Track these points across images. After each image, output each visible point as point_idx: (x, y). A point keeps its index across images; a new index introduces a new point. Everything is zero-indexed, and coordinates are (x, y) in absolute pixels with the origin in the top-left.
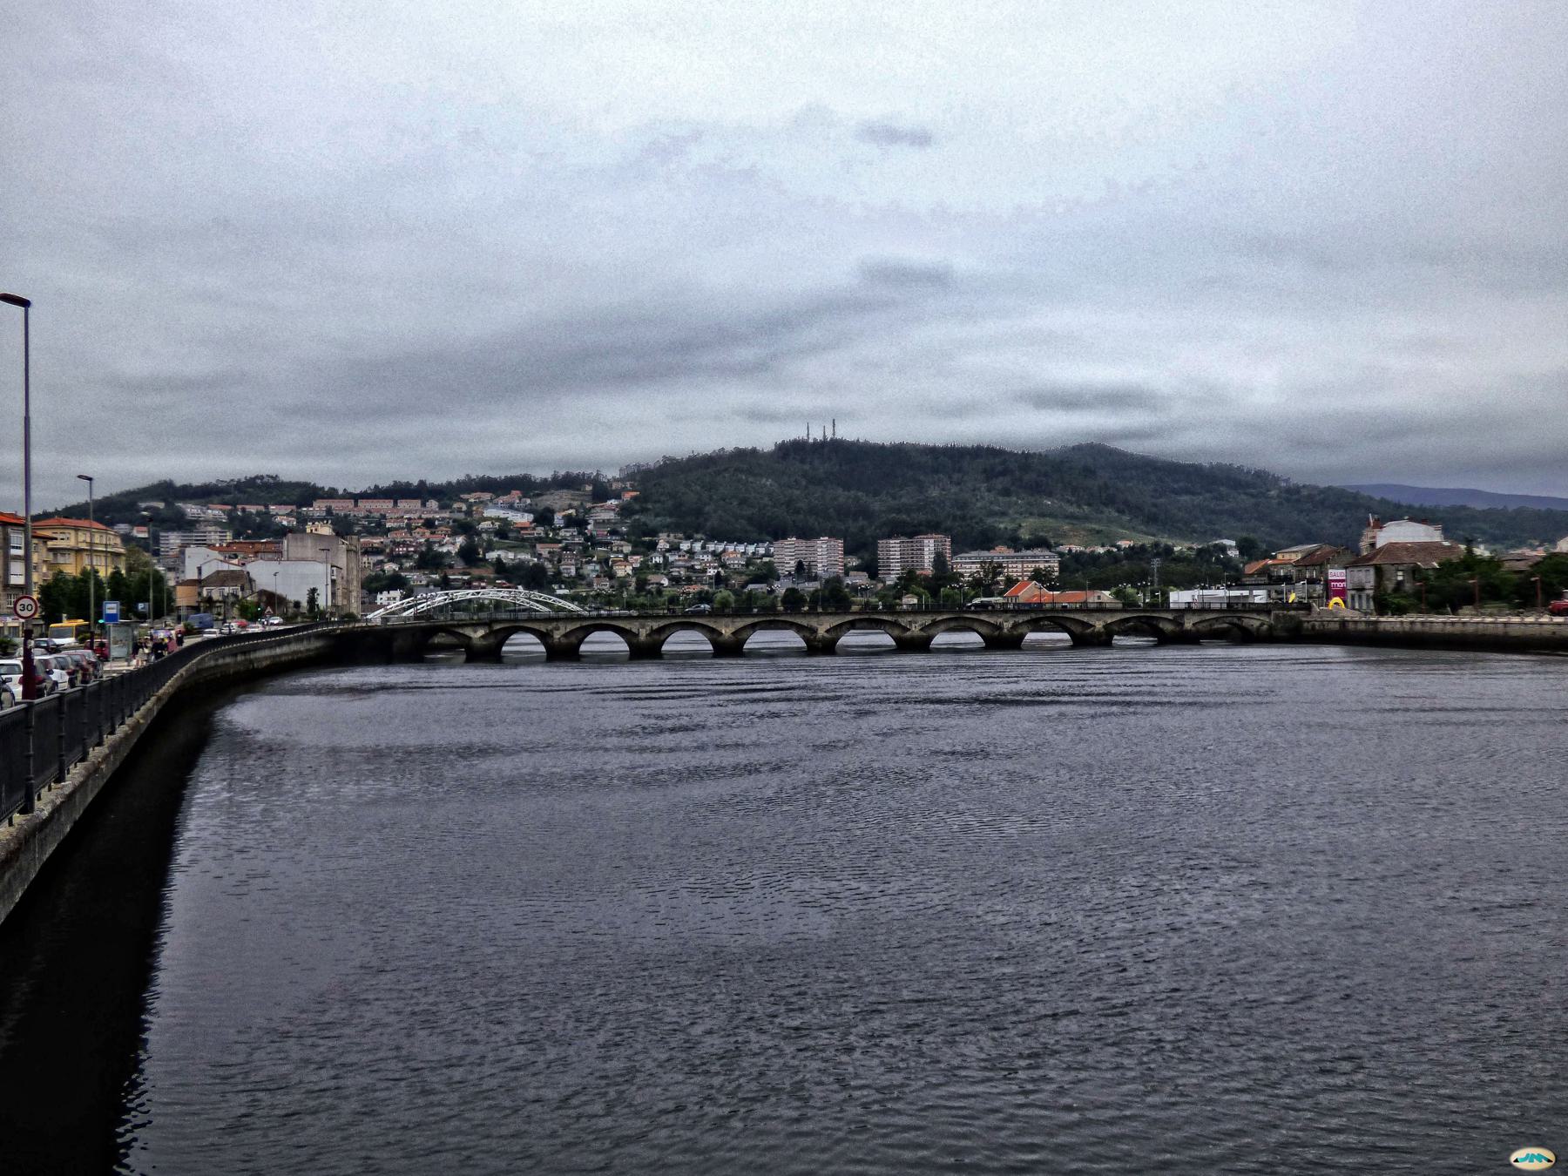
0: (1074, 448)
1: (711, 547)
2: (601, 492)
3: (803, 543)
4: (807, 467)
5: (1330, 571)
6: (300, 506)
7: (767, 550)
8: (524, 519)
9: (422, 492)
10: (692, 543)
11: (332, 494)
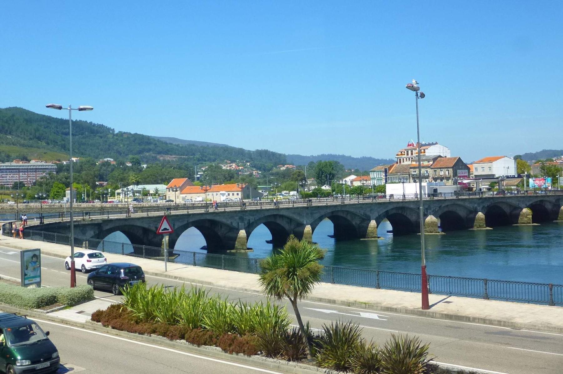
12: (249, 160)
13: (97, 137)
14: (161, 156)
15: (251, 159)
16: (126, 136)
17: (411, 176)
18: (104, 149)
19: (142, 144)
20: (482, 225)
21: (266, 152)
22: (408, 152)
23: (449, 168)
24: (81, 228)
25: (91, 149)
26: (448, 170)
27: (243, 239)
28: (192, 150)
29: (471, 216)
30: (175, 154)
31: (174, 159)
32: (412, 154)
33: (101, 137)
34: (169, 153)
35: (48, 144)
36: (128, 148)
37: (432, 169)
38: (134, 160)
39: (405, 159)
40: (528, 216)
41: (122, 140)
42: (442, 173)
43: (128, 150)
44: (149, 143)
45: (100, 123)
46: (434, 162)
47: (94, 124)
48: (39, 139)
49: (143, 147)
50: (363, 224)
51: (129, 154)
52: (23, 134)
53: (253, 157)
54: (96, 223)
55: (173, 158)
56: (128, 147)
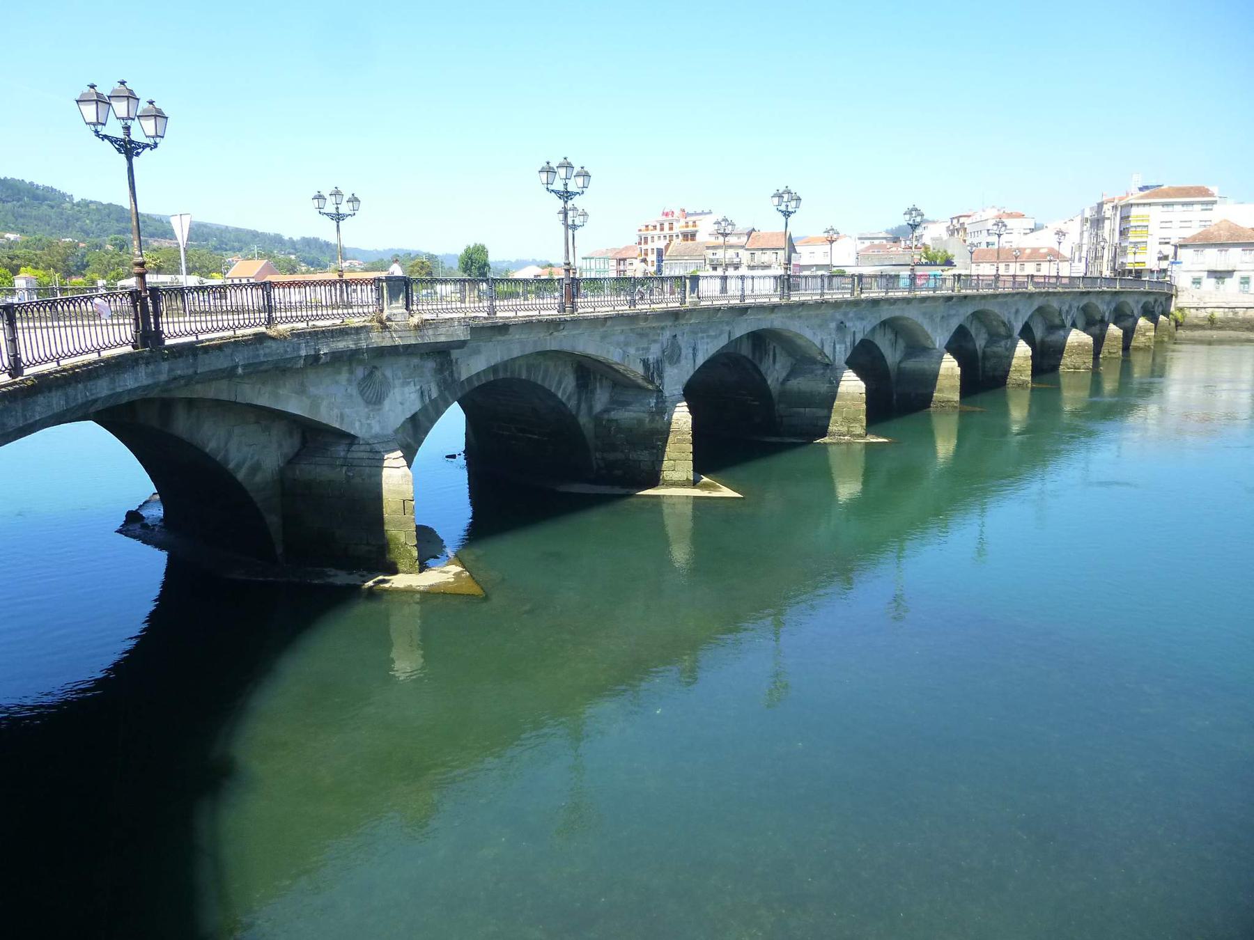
12: (292, 251)
13: (45, 207)
14: (155, 241)
15: (296, 249)
16: (95, 207)
17: (707, 262)
18: (58, 225)
19: (121, 220)
20: (1115, 351)
21: (316, 240)
22: (662, 225)
23: (778, 249)
24: (360, 372)
26: (777, 253)
27: (853, 399)
28: (203, 233)
32: (671, 229)
33: (52, 207)
34: (168, 236)
37: (747, 249)
38: (118, 242)
39: (656, 238)
40: (1147, 334)
41: (88, 213)
43: (99, 229)
45: (46, 185)
47: (37, 186)
49: (123, 225)
50: (995, 349)
53: (297, 246)
54: (442, 339)
56: (99, 224)
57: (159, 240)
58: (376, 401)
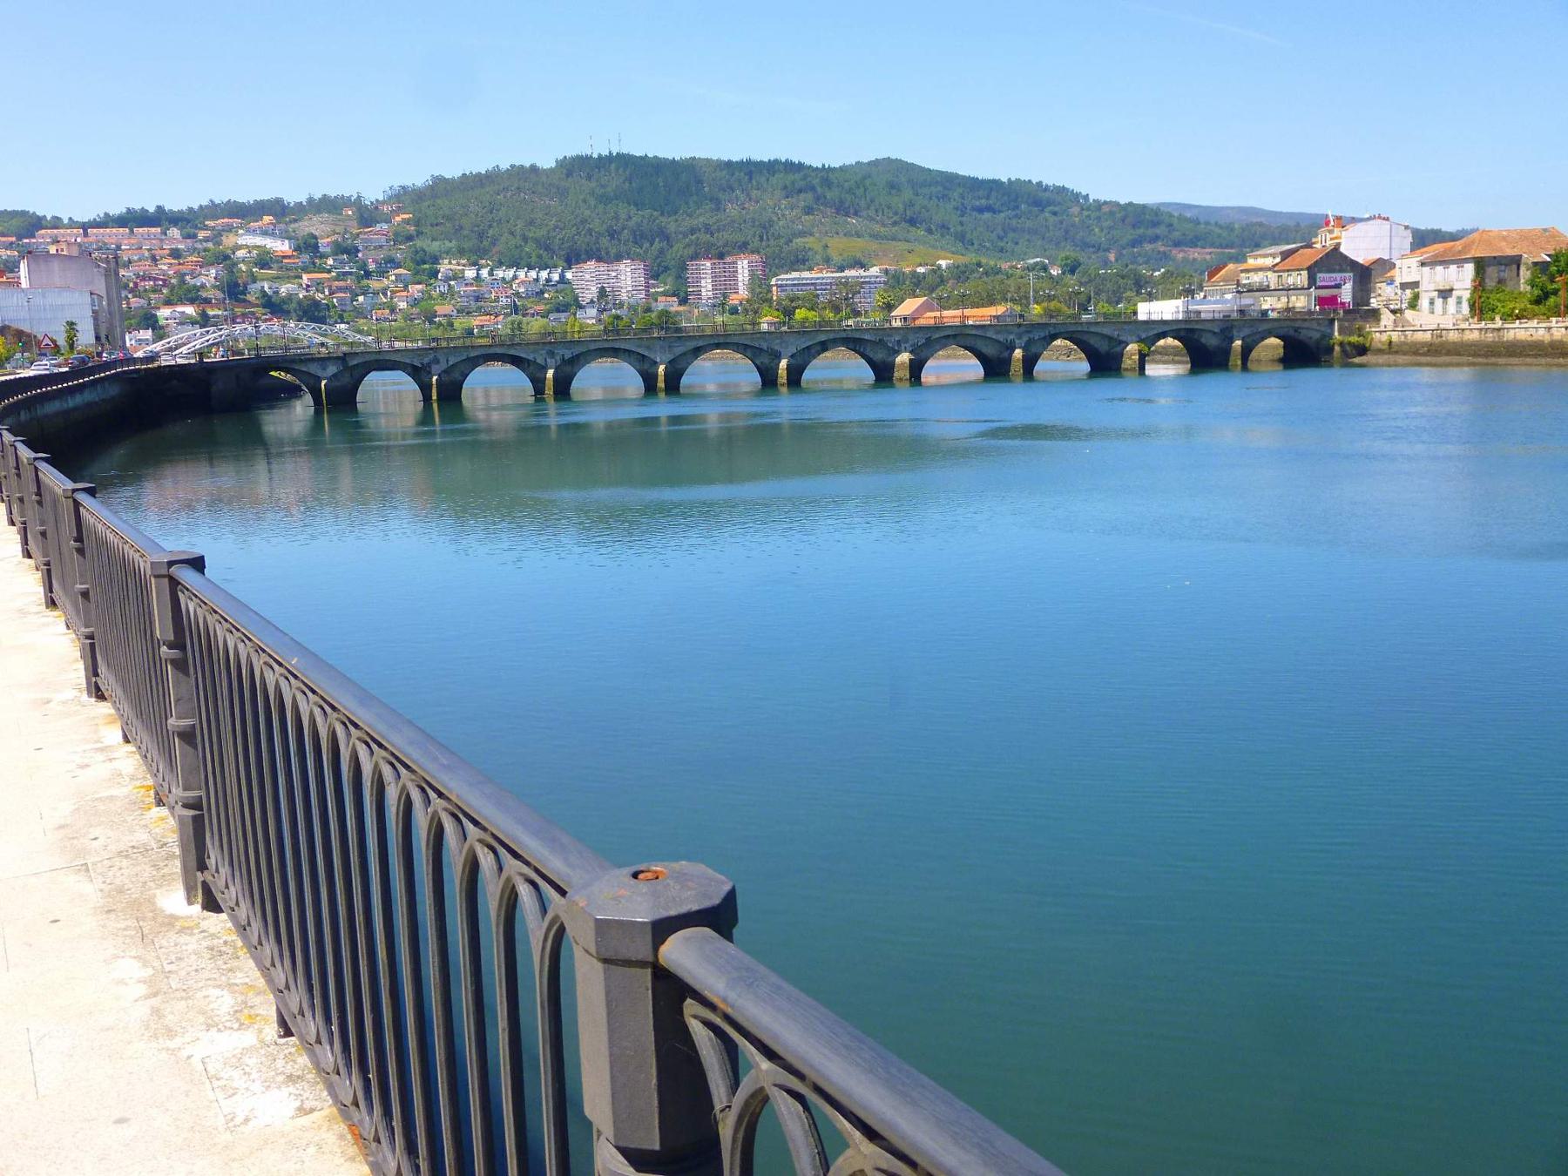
0: (870, 163)
1: (500, 273)
2: (368, 215)
3: (603, 267)
4: (593, 184)
5: (1319, 275)
6: (20, 238)
7: (562, 276)
8: (281, 246)
9: (159, 218)
10: (478, 270)
11: (56, 223)
25: (1028, 240)
29: (1006, 354)
30: (1212, 245)
31: (1208, 257)
33: (1055, 214)
34: (1199, 243)
35: (930, 231)
36: (1110, 236)
37: (1275, 272)
38: (1069, 261)
41: (1099, 218)
42: (1291, 281)
44: (1155, 224)
46: (1282, 260)
47: (1047, 185)
48: (912, 222)
51: (1110, 248)
52: (880, 214)
55: (1207, 253)
57: (1186, 249)
58: (324, 369)
